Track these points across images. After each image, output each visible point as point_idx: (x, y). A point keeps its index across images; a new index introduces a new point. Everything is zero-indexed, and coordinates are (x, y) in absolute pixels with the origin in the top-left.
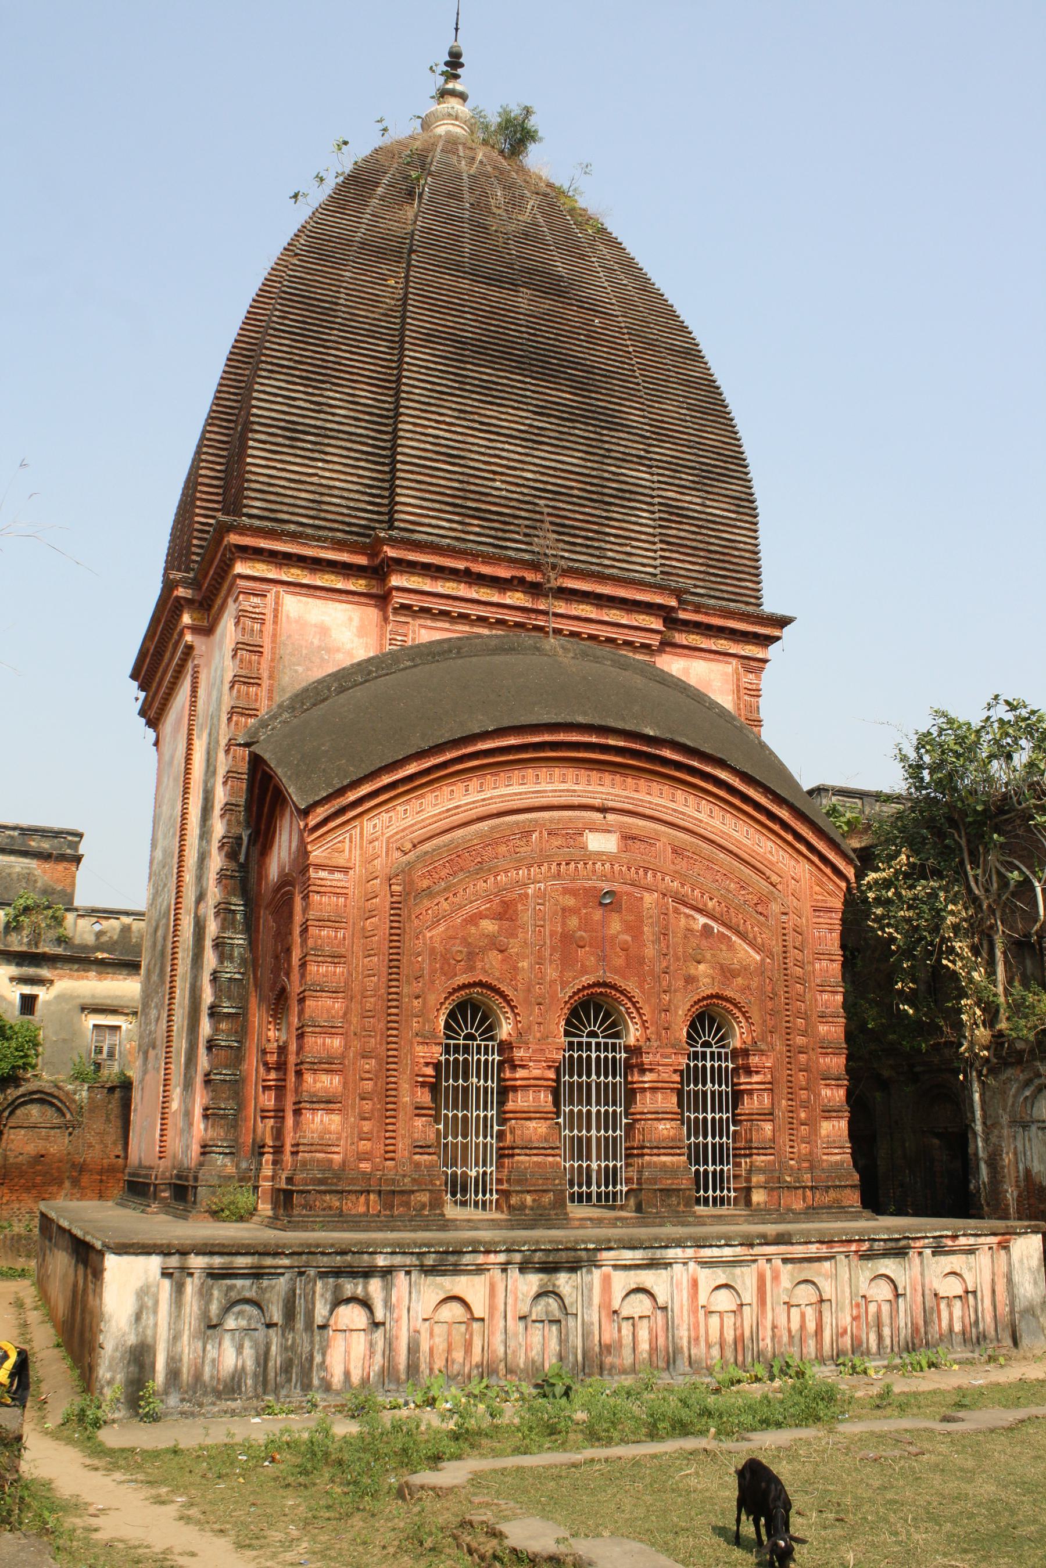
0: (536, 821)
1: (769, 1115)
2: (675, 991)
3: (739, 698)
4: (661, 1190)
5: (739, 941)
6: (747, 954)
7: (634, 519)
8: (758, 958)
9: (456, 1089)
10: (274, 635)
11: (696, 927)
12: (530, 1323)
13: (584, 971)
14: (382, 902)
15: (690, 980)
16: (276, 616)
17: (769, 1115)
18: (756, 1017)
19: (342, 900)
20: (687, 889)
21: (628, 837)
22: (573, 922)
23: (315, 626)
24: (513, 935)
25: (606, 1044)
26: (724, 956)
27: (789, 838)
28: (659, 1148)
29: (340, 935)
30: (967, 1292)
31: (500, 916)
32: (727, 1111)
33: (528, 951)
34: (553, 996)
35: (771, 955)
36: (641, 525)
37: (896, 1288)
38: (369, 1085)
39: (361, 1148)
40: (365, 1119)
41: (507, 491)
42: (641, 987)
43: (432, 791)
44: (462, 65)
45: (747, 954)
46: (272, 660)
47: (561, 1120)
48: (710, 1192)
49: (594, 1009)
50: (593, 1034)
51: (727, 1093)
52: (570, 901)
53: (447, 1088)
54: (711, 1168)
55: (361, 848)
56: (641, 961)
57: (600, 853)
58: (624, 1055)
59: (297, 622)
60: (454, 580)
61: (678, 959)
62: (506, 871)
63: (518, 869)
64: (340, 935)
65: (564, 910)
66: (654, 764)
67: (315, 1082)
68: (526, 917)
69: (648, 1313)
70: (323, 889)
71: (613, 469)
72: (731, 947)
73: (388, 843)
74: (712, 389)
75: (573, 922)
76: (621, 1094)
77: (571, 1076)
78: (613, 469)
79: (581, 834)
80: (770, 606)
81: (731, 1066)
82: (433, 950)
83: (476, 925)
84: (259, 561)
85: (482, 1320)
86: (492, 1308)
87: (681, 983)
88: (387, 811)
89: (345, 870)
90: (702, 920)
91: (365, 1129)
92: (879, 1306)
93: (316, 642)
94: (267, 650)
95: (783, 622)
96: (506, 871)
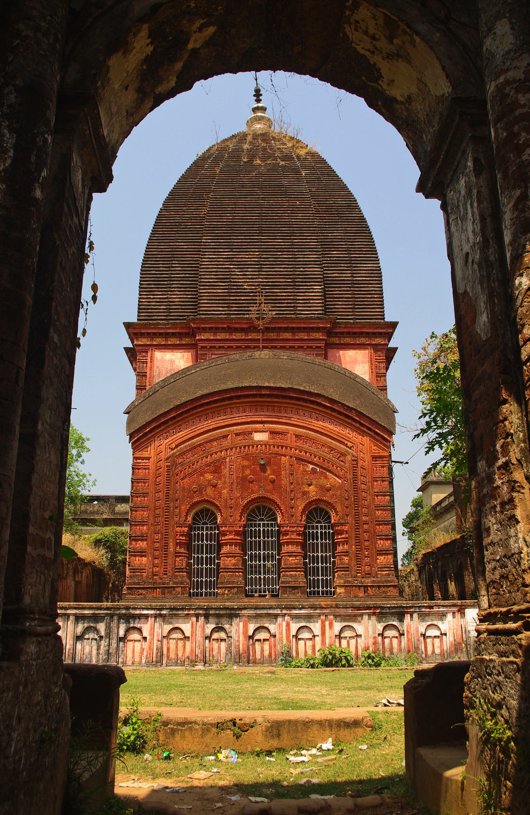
0: (230, 431)
1: (346, 554)
2: (297, 499)
3: (371, 364)
4: (289, 587)
5: (331, 474)
6: (334, 480)
7: (312, 290)
8: (340, 481)
9: (198, 545)
10: (151, 367)
11: (308, 469)
12: (211, 640)
13: (253, 492)
14: (164, 470)
15: (305, 493)
16: (151, 359)
17: (346, 554)
18: (339, 509)
19: (147, 471)
20: (303, 453)
21: (273, 433)
22: (248, 472)
23: (168, 361)
24: (220, 479)
25: (268, 524)
26: (322, 481)
27: (358, 425)
28: (290, 569)
29: (147, 485)
30: (441, 634)
31: (214, 472)
32: (330, 552)
33: (226, 486)
34: (237, 504)
35: (345, 478)
36: (315, 292)
37: (399, 631)
38: (157, 545)
39: (154, 570)
40: (156, 558)
41: (250, 289)
42: (280, 498)
43: (184, 423)
44: (261, 95)
45: (334, 480)
46: (150, 378)
47: (247, 557)
48: (320, 589)
49: (261, 509)
50: (262, 520)
51: (329, 544)
52: (246, 463)
53: (195, 545)
54: (320, 578)
55: (154, 449)
56: (280, 486)
57: (259, 441)
58: (277, 528)
59: (160, 361)
60: (224, 332)
61: (299, 484)
62: (216, 453)
63: (221, 451)
64: (147, 485)
65: (243, 466)
66: (286, 399)
67: (136, 544)
68: (226, 472)
69: (268, 638)
70: (139, 467)
71: (301, 269)
72: (326, 477)
73: (165, 446)
74: (363, 219)
75: (248, 472)
76: (248, 545)
77: (251, 538)
78: (301, 269)
79: (251, 434)
80: (389, 318)
81: (331, 531)
82: (184, 488)
83: (203, 476)
84: (143, 338)
85: (189, 637)
86: (192, 632)
87: (299, 495)
88: (165, 433)
89: (148, 459)
90: (311, 466)
91: (156, 562)
92: (391, 640)
93: (169, 368)
94: (148, 374)
95: (394, 325)
96: (216, 453)
